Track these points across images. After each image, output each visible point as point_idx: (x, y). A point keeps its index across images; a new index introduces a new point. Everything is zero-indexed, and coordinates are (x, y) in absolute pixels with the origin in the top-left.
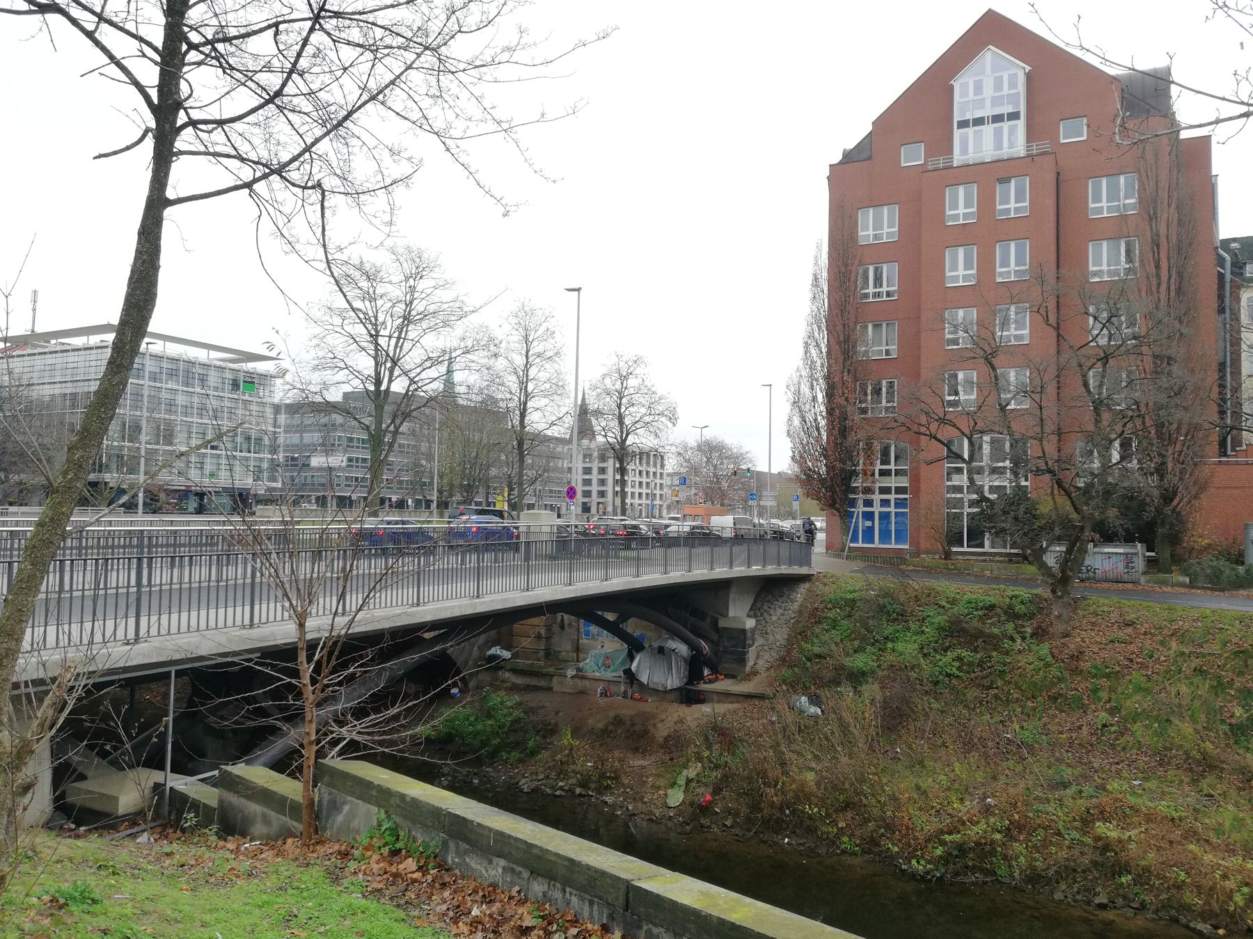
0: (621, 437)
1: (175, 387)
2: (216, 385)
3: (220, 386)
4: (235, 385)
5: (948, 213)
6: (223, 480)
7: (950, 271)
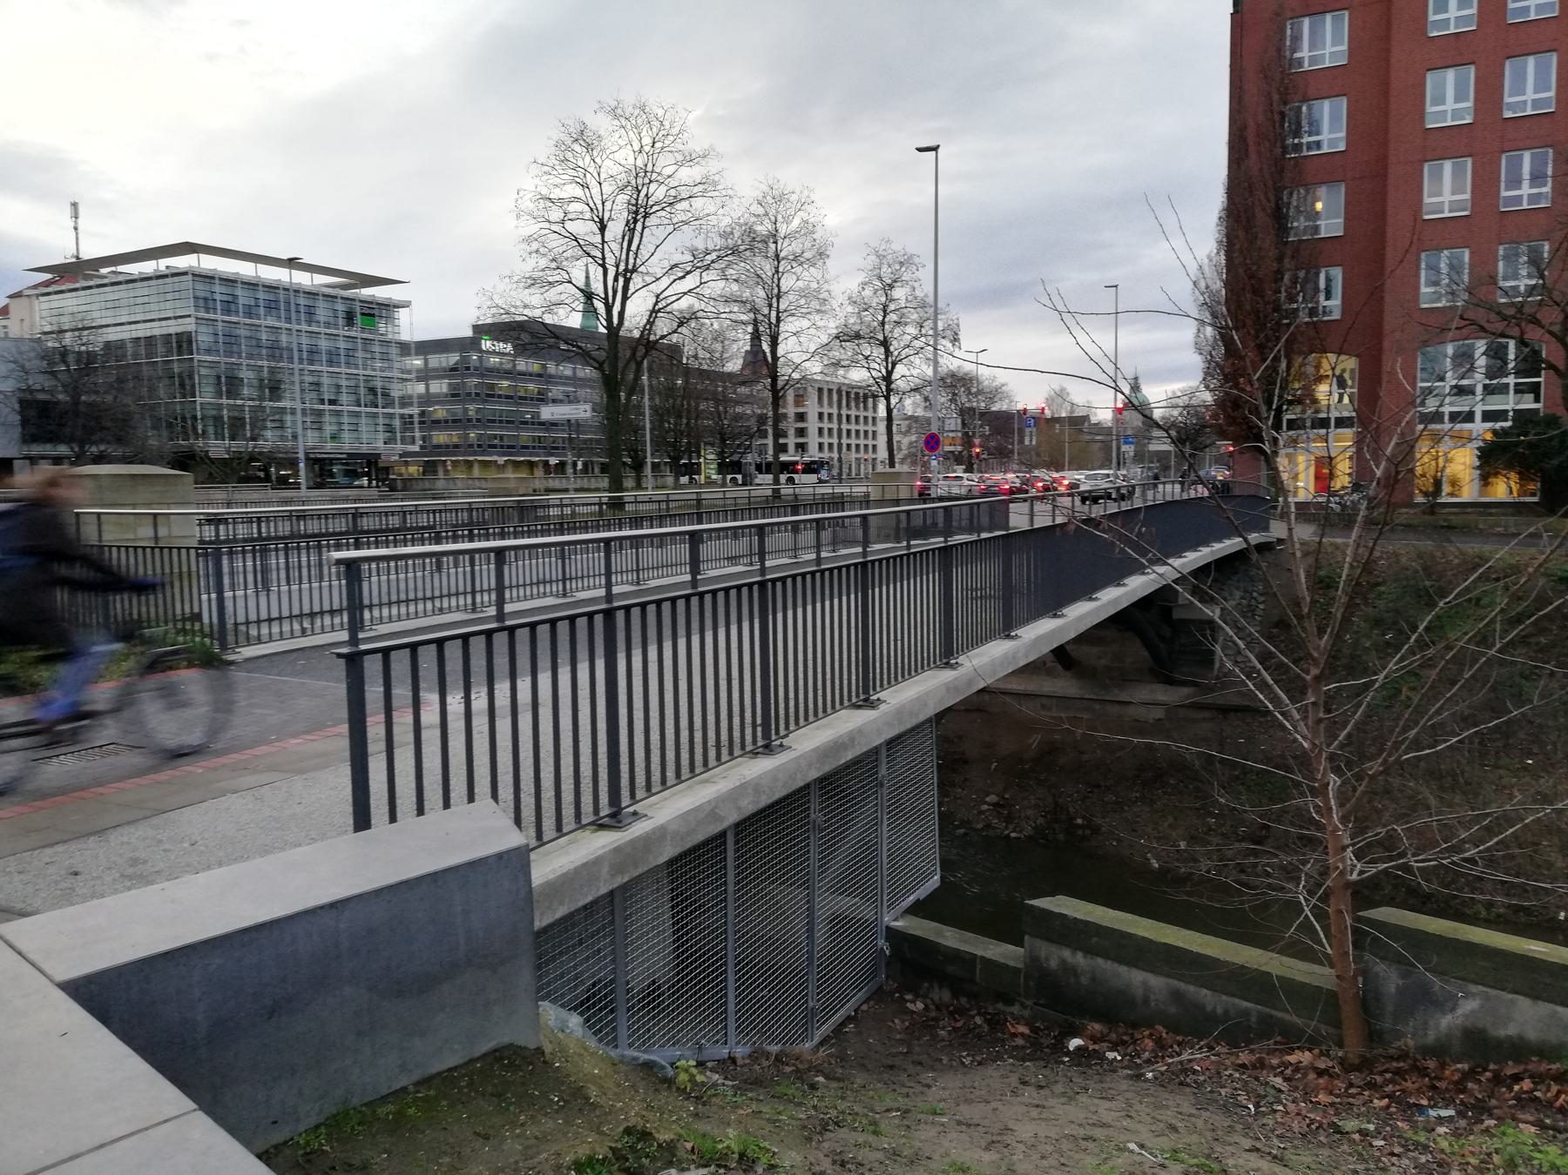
0: (887, 368)
1: (277, 324)
2: (326, 319)
3: (332, 320)
4: (350, 318)
5: (1432, 17)
6: (347, 444)
7: (1510, 96)
